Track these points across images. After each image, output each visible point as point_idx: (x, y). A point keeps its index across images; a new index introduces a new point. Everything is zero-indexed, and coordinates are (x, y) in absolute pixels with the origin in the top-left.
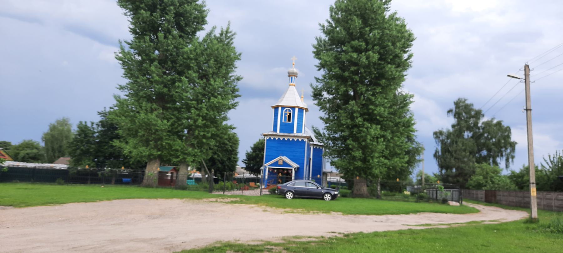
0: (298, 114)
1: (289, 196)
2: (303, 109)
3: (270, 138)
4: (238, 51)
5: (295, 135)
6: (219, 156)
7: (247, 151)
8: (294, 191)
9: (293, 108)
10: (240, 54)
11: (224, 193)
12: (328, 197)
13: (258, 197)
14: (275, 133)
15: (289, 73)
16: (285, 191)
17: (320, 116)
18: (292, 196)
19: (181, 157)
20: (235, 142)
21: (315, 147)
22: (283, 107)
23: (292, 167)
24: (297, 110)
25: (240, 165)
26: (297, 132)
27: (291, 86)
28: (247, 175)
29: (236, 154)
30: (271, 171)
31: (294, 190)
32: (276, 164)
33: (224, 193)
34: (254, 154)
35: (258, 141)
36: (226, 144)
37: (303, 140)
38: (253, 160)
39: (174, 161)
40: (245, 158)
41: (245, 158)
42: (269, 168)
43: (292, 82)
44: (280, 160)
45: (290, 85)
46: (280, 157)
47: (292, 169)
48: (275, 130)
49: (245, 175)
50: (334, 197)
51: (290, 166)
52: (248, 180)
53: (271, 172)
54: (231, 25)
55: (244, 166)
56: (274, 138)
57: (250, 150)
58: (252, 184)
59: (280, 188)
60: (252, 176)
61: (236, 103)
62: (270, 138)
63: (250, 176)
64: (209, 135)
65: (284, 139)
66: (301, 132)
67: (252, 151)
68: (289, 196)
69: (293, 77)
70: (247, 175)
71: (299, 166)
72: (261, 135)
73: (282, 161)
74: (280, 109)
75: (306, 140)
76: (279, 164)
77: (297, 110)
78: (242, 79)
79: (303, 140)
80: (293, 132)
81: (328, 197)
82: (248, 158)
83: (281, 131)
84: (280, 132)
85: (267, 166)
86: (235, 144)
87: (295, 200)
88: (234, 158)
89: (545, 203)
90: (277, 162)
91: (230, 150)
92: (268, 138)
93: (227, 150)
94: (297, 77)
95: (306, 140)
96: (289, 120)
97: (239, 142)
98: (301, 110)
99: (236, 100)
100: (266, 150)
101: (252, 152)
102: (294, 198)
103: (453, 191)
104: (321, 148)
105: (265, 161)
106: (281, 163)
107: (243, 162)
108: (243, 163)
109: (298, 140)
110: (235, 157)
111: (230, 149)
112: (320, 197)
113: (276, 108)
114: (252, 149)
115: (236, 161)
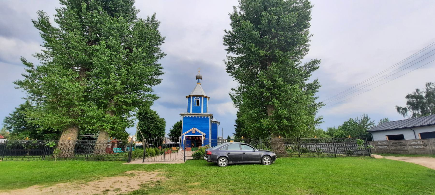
0: (203, 101)
1: (223, 162)
2: (207, 98)
3: (186, 117)
4: (162, 35)
5: (202, 114)
6: (153, 132)
7: (170, 129)
8: (228, 157)
9: (200, 97)
10: (164, 38)
11: (143, 161)
12: (267, 160)
13: (181, 165)
14: (189, 113)
15: (196, 77)
16: (217, 158)
17: (138, 184)
18: (226, 163)
19: (97, 125)
20: (163, 123)
21: (212, 123)
22: (194, 96)
23: (202, 135)
24: (203, 98)
25: (167, 136)
26: (203, 112)
27: (198, 85)
28: (170, 142)
29: (164, 131)
30: (187, 138)
31: (228, 155)
32: (191, 133)
33: (143, 161)
34: (174, 130)
35: (177, 122)
36: (158, 125)
37: (207, 117)
38: (174, 134)
39: (89, 129)
40: (169, 133)
41: (169, 133)
42: (185, 136)
43: (198, 82)
44: (193, 131)
45: (197, 84)
46: (193, 128)
47: (202, 136)
48: (189, 111)
49: (169, 143)
50: (273, 159)
51: (201, 135)
52: (171, 146)
53: (188, 138)
54: (156, 16)
55: (169, 137)
56: (189, 117)
57: (172, 128)
58: (174, 148)
59: (210, 153)
60: (173, 143)
61: (160, 80)
62: (186, 117)
63: (172, 143)
64: (130, 101)
65: (195, 117)
66: (206, 112)
67: (173, 129)
68: (223, 162)
69: (199, 79)
70: (170, 142)
71: (205, 134)
72: (180, 115)
73: (194, 131)
74: (192, 97)
75: (209, 117)
76: (193, 133)
77: (203, 98)
78: (165, 55)
79: (207, 117)
80: (201, 112)
81: (267, 160)
82: (171, 133)
83: (193, 111)
84: (192, 112)
85: (184, 135)
86: (163, 125)
87: (229, 167)
88: (163, 133)
89: (393, 148)
90: (191, 132)
91: (160, 128)
92: (184, 117)
93: (158, 128)
94: (201, 79)
95: (209, 117)
96: (198, 104)
97: (166, 123)
98: (205, 98)
99: (160, 77)
100: (183, 124)
101: (173, 130)
102: (228, 164)
103: (316, 145)
104: (216, 123)
105: (183, 132)
106: (194, 132)
107: (168, 135)
108: (168, 135)
109: (204, 117)
110: (163, 132)
111: (160, 127)
112: (258, 162)
113: (189, 97)
114: (173, 127)
115: (164, 135)
